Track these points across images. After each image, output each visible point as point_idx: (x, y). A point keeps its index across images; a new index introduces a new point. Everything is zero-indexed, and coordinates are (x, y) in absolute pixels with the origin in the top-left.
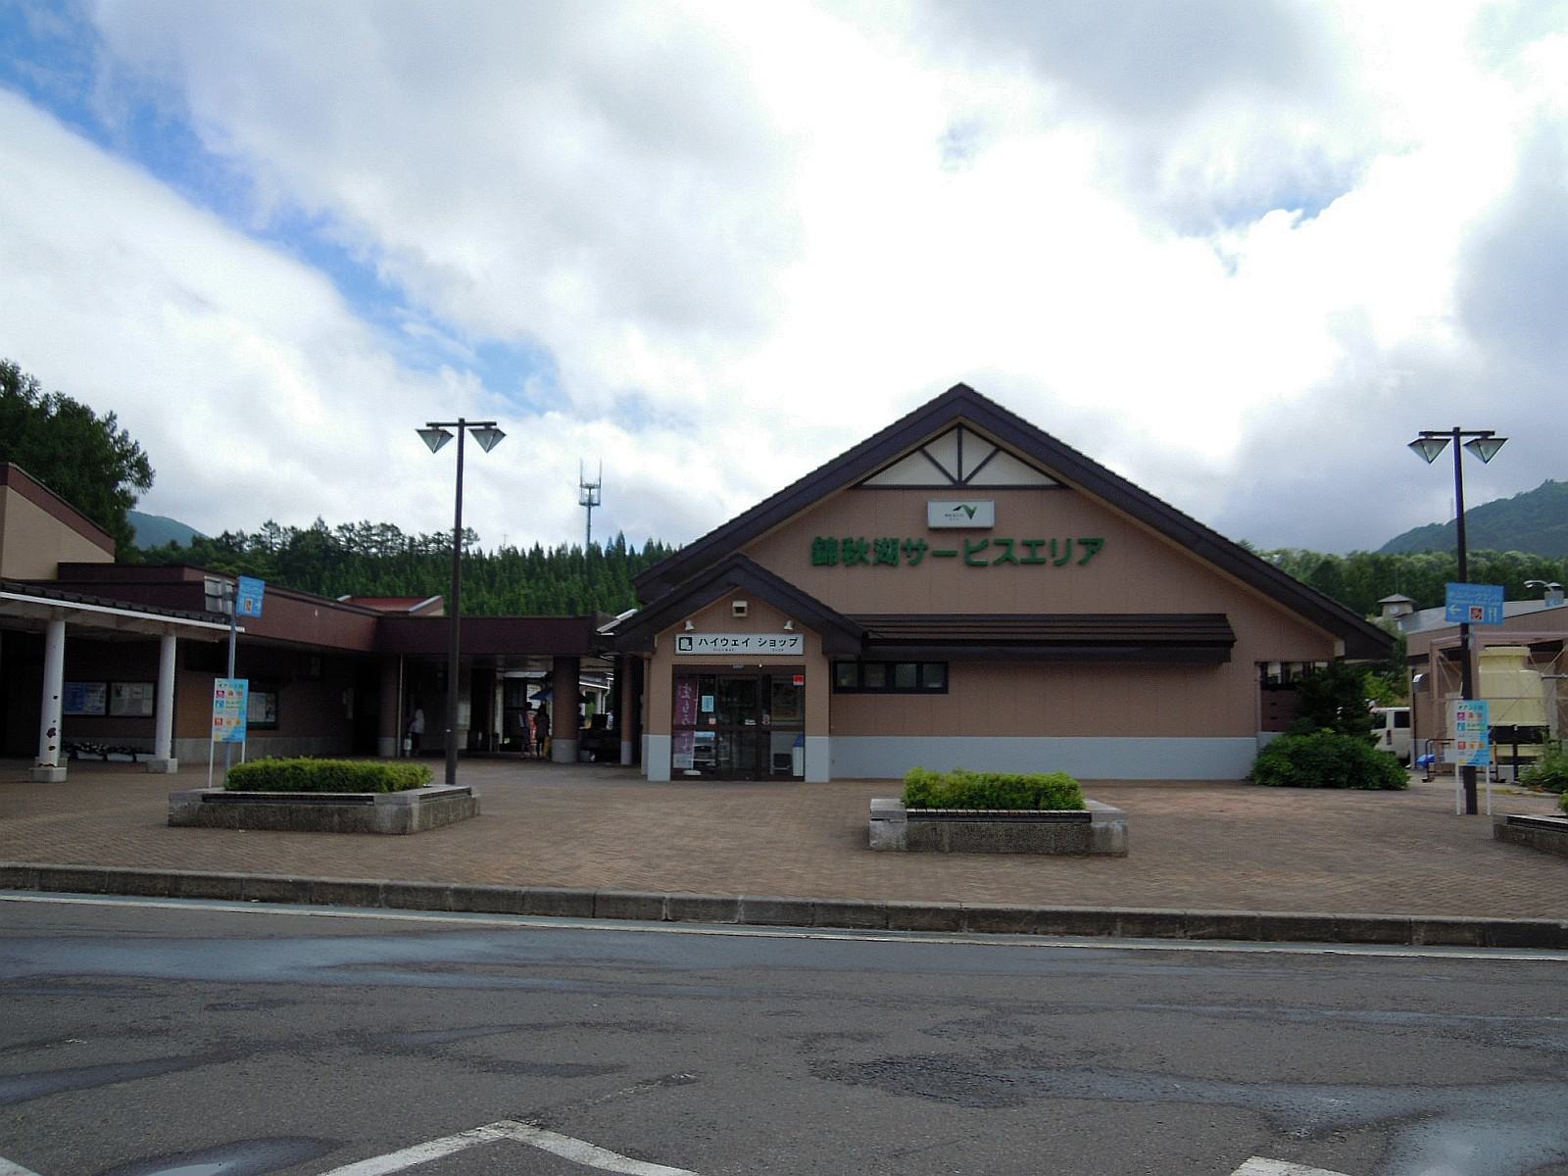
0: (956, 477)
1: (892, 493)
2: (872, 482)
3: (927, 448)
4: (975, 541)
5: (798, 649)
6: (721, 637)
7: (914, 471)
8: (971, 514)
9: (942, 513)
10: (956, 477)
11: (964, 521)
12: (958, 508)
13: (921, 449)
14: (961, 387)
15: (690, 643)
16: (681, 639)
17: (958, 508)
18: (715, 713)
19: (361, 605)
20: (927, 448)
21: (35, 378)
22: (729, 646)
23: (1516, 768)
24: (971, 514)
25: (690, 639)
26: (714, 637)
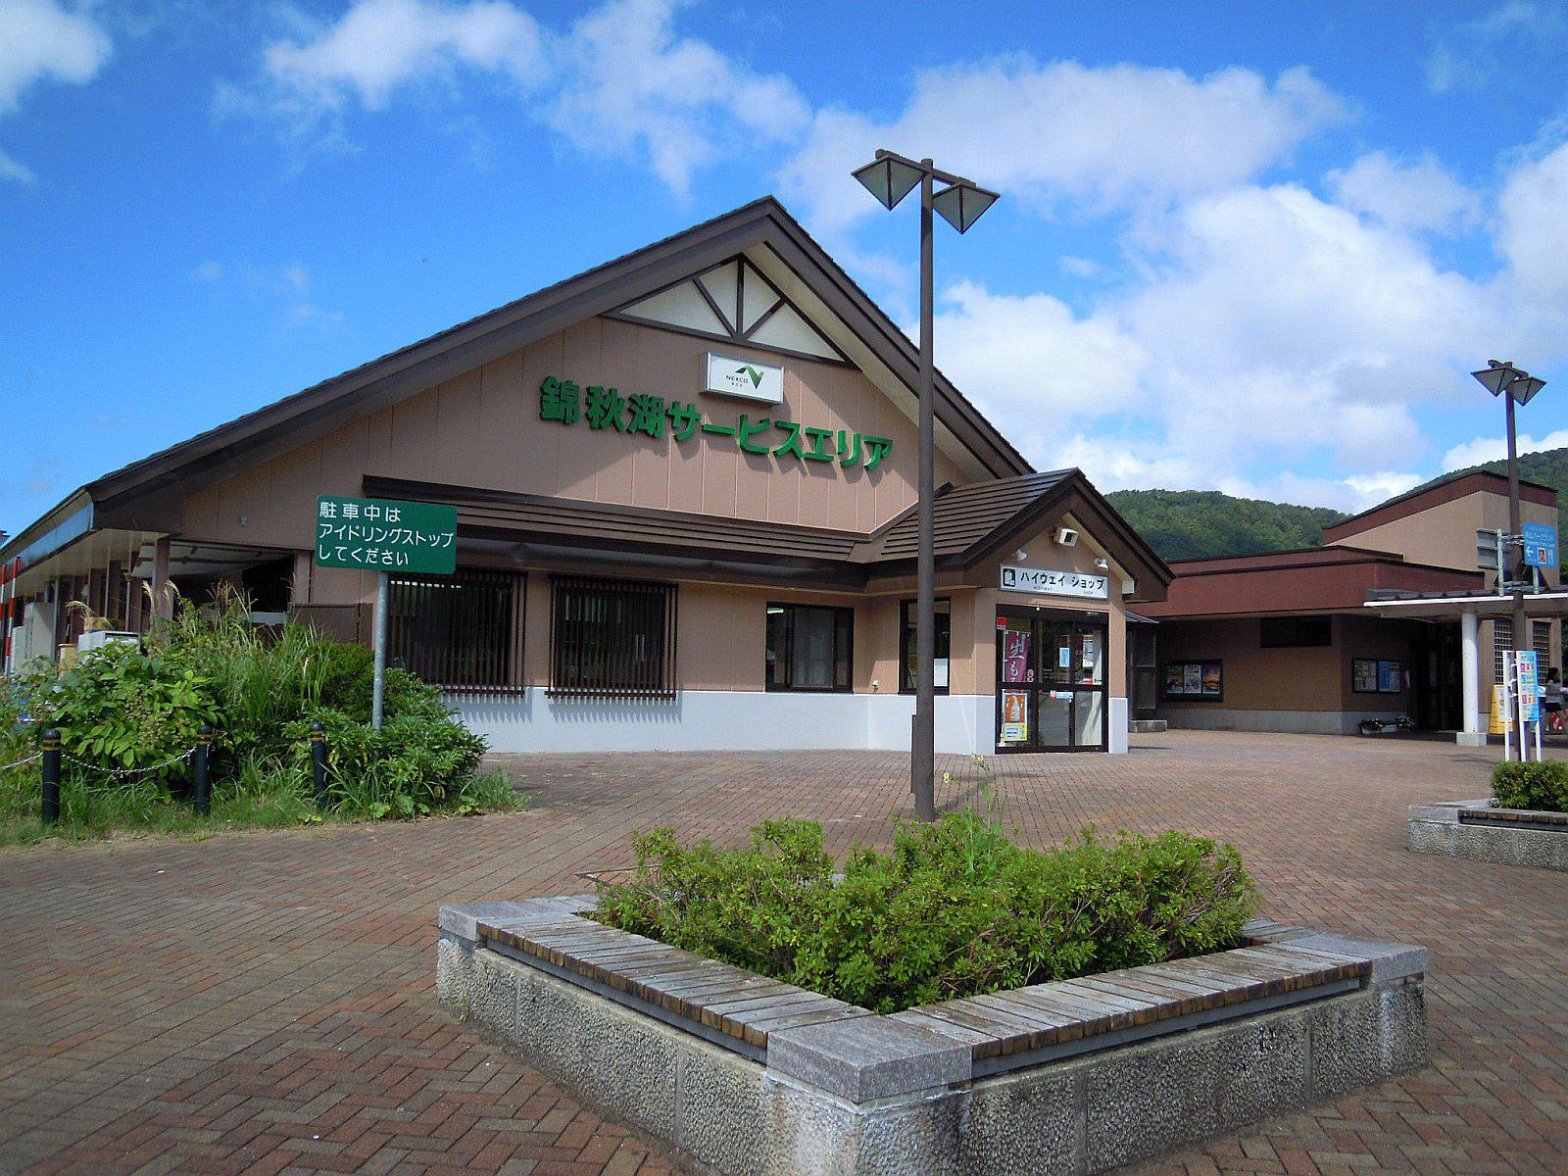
0: (746, 328)
1: (656, 332)
2: (642, 311)
3: (704, 279)
4: (754, 417)
5: (1102, 594)
6: (1041, 572)
7: (687, 311)
8: (757, 381)
9: (723, 374)
10: (746, 328)
11: (747, 390)
12: (742, 371)
13: (693, 278)
14: (1199, 80)
15: (1014, 578)
16: (1005, 570)
17: (742, 371)
18: (455, 588)
19: (233, 553)
20: (704, 279)
21: (552, 714)
22: (1047, 585)
23: (1377, 665)
24: (757, 381)
25: (1013, 572)
26: (1035, 572)
